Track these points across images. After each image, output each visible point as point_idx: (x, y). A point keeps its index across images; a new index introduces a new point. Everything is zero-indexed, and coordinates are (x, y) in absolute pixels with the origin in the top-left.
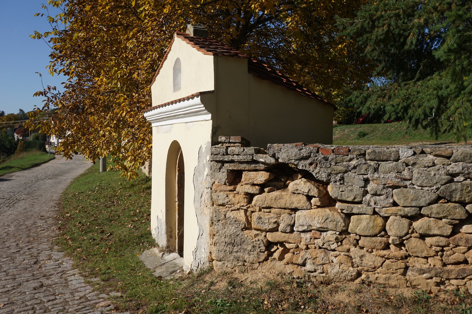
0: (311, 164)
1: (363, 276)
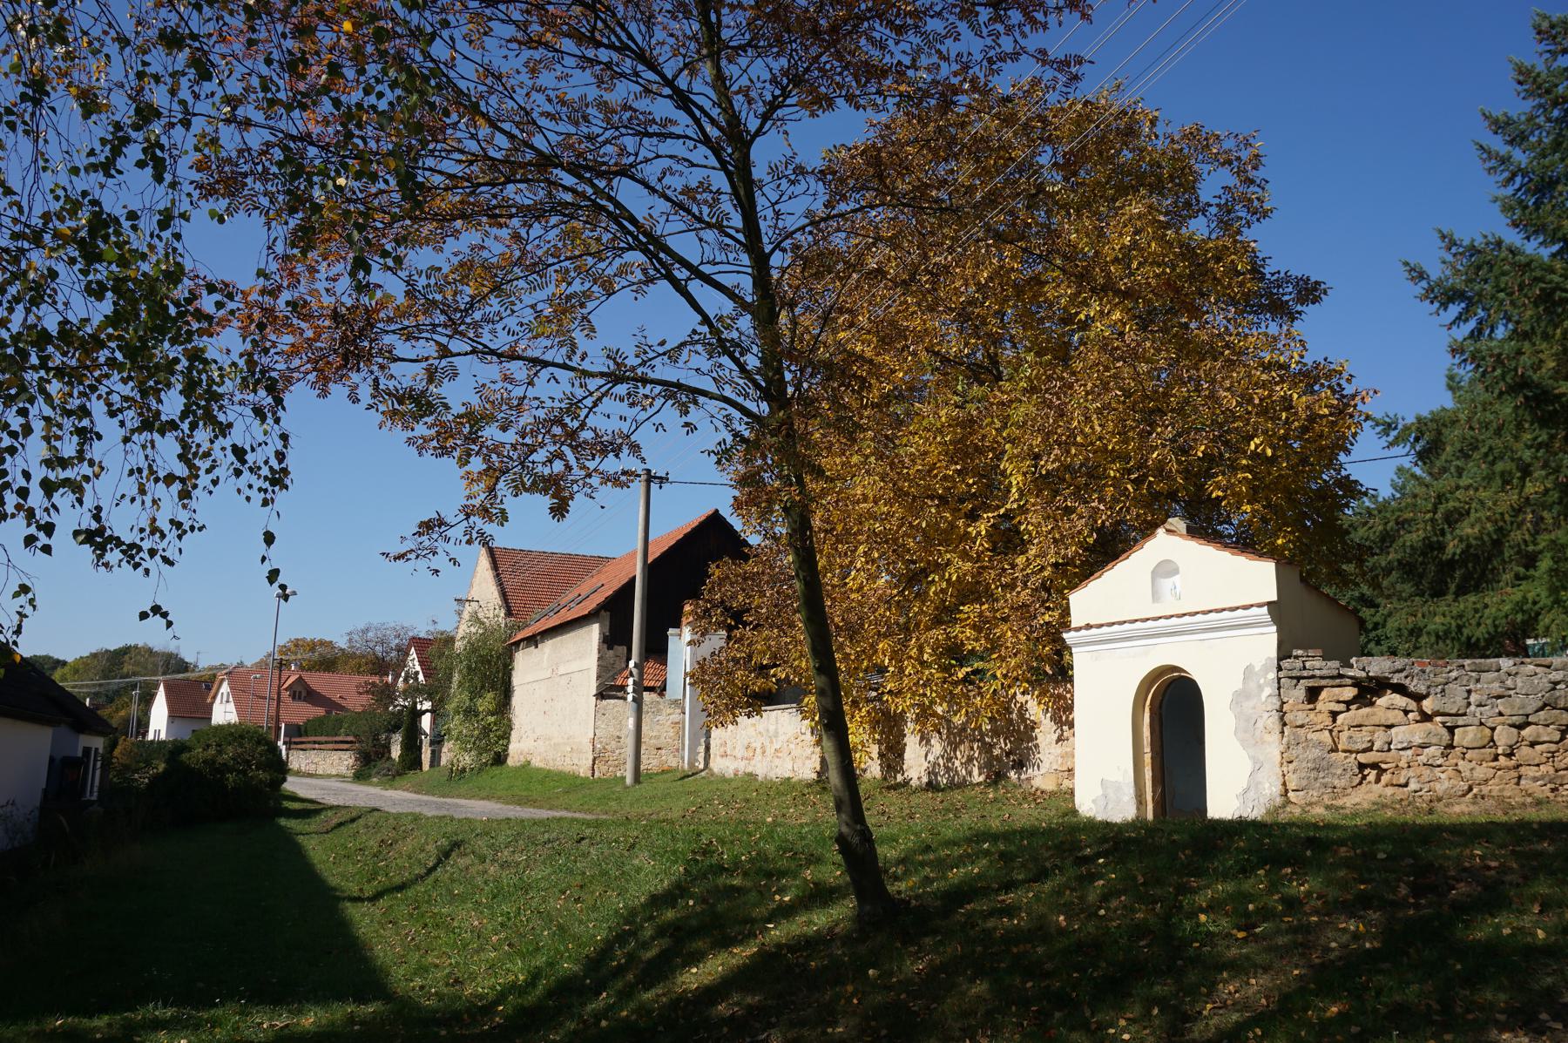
1: (1475, 790)
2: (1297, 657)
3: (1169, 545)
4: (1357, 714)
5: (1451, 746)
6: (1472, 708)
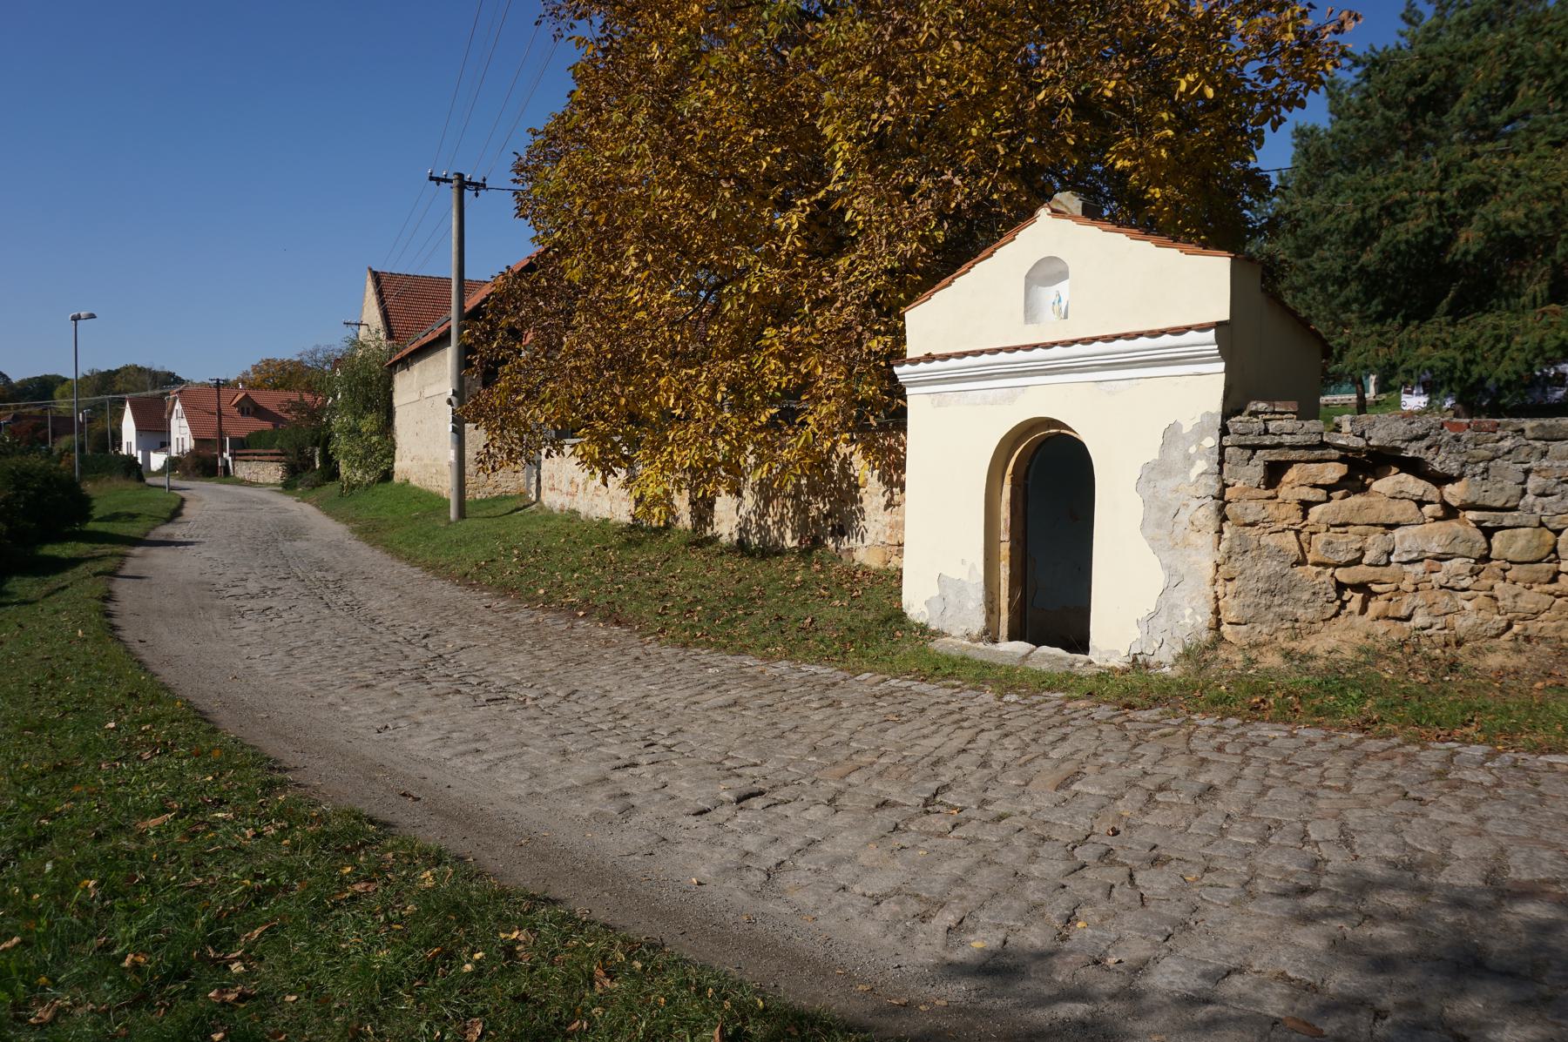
0: (1428, 448)
1: (1516, 628)
2: (1255, 414)
3: (1053, 233)
4: (1344, 506)
5: (1485, 559)
6: (1530, 498)
